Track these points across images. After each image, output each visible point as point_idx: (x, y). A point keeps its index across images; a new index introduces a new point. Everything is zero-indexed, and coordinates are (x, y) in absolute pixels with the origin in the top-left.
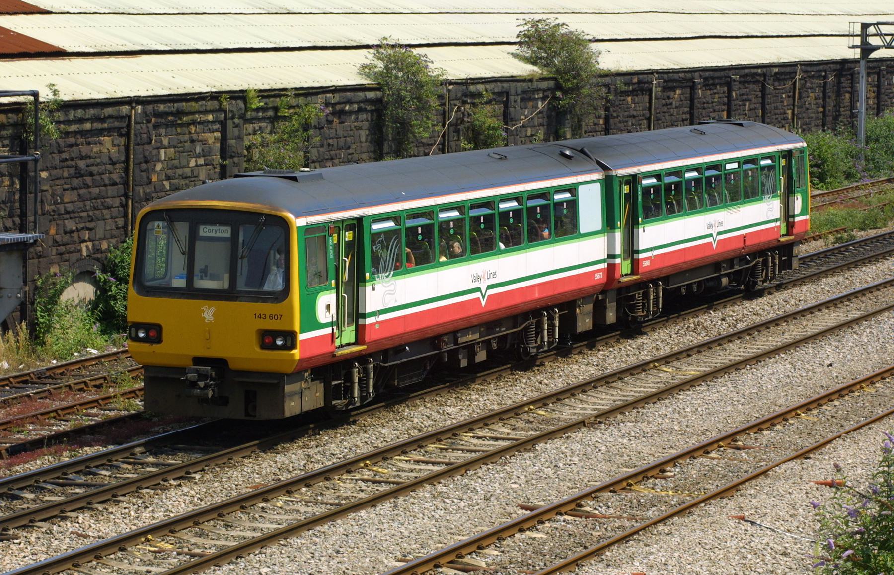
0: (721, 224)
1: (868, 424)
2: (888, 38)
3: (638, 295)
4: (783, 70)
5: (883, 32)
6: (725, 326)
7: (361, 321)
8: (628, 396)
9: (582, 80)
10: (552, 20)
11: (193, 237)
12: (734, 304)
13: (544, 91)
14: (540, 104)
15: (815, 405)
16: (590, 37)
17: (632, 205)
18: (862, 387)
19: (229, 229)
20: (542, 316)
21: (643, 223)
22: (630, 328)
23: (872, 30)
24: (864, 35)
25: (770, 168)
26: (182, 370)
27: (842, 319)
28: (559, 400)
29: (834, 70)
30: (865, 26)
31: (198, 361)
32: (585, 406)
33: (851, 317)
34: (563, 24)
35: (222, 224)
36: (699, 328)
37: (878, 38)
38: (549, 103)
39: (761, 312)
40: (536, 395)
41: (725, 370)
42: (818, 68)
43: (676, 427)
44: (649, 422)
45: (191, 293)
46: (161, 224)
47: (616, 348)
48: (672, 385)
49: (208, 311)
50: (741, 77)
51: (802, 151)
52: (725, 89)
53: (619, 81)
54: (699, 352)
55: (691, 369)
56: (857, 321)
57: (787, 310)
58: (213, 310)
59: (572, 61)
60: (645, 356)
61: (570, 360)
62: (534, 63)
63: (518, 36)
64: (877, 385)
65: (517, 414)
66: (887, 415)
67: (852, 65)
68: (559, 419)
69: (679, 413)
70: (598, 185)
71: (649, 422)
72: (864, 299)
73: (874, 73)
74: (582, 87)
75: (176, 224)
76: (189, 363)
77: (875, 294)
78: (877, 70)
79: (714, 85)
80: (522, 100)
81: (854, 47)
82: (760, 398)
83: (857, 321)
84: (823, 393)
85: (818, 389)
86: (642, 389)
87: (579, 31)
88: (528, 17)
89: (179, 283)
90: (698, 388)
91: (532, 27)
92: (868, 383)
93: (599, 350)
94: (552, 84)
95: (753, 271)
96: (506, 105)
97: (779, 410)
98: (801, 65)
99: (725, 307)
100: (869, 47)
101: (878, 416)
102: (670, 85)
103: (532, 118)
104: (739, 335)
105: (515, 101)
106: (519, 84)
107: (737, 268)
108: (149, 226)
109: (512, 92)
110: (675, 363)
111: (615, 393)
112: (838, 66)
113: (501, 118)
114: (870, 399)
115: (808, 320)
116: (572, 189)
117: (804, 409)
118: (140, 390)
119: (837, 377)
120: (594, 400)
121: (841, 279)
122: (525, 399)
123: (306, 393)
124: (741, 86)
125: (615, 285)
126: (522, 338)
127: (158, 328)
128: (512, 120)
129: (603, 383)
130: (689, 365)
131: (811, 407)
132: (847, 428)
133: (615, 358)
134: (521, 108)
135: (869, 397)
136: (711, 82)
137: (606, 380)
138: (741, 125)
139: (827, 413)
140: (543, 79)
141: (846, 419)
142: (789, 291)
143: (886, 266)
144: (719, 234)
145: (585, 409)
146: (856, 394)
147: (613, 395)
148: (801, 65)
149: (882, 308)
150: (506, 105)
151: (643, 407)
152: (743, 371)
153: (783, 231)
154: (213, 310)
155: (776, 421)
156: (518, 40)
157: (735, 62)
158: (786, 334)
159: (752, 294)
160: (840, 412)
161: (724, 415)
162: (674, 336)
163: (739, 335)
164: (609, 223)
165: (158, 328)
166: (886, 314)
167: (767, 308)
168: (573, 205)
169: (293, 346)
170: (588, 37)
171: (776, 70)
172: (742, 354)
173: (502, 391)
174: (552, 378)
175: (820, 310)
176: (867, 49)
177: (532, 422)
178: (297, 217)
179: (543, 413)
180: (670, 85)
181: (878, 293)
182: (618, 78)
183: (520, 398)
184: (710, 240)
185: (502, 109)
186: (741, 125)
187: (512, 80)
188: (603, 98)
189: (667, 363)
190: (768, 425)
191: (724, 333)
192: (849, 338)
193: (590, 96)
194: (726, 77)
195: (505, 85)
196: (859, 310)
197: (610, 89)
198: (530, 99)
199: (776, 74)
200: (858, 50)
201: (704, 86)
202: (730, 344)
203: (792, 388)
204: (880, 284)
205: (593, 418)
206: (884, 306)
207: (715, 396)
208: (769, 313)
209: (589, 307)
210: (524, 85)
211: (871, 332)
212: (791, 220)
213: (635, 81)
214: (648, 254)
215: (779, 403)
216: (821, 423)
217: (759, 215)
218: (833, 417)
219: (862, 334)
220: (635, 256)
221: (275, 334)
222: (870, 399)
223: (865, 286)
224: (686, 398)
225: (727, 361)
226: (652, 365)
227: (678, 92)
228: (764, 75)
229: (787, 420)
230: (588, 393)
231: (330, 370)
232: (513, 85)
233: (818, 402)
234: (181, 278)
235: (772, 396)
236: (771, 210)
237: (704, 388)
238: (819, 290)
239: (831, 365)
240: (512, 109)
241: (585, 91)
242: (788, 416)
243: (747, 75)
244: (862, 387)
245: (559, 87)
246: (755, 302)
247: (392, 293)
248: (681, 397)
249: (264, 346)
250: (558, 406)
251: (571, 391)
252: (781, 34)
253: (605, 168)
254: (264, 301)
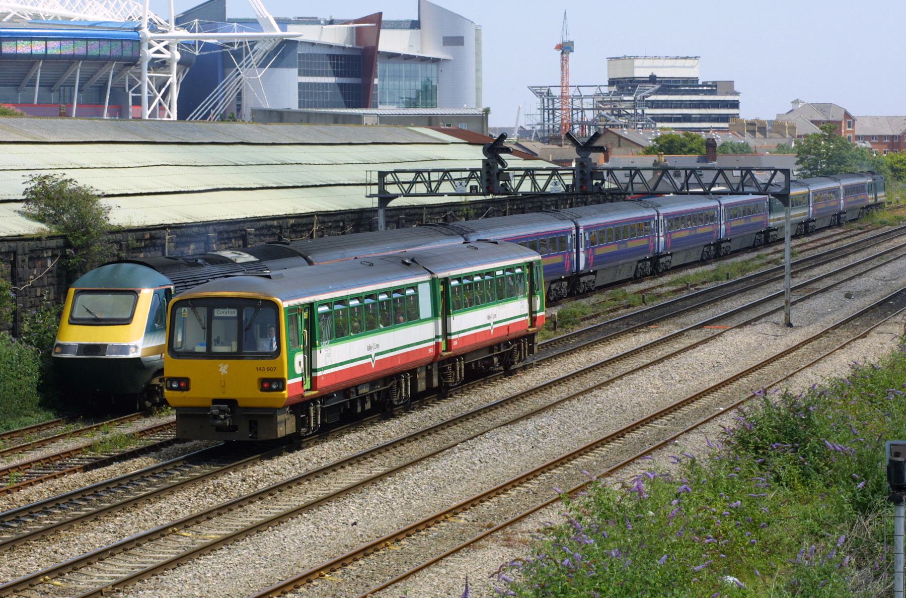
0: (378, 345)
1: (394, 583)
2: (406, 186)
3: (449, 366)
4: (299, 221)
5: (401, 180)
6: (246, 486)
7: (314, 374)
8: (146, 563)
9: (92, 237)
10: (59, 175)
11: (210, 317)
12: (254, 464)
13: (53, 249)
14: (49, 262)
15: (339, 565)
16: (99, 193)
17: (448, 300)
18: (387, 545)
19: (236, 311)
20: (401, 377)
21: (454, 313)
22: (442, 393)
23: (389, 178)
24: (382, 183)
25: (521, 274)
26: (208, 409)
27: (366, 475)
28: (75, 569)
29: (352, 220)
30: (382, 175)
31: (216, 401)
32: (103, 574)
33: (374, 473)
34: (71, 180)
35: (230, 307)
36: (219, 490)
37: (396, 186)
38: (59, 262)
39: (282, 471)
40: (51, 566)
41: (247, 532)
42: (335, 218)
43: (197, 593)
44: (169, 589)
45: (210, 355)
46: (186, 309)
47: (133, 513)
48: (192, 550)
49: (223, 367)
50: (256, 229)
51: (538, 262)
52: (241, 243)
53: (130, 237)
54: (220, 514)
55: (211, 532)
56: (381, 477)
57: (309, 468)
58: (226, 366)
59: (82, 217)
60: (163, 521)
61: (86, 527)
62: (42, 221)
63: (24, 194)
64: (403, 542)
65: (32, 586)
66: (413, 573)
67: (371, 215)
68: (75, 590)
69: (200, 578)
70: (428, 284)
71: (169, 589)
72: (387, 454)
73: (393, 222)
74: (92, 245)
75: (197, 308)
76: (209, 403)
77: (399, 449)
78: (396, 218)
79: (230, 239)
80: (31, 259)
81: (371, 196)
82: (283, 561)
83: (381, 477)
84: (347, 552)
85: (342, 549)
86: (161, 555)
87: (88, 187)
88: (34, 174)
89: (201, 349)
90: (219, 552)
91: (39, 184)
92: (393, 540)
93: (116, 516)
94: (61, 242)
95: (511, 354)
96: (14, 264)
97: (303, 572)
98: (318, 215)
99: (245, 467)
100: (387, 195)
101: (404, 574)
102: (183, 239)
103: (41, 278)
104: (259, 496)
105: (23, 261)
106: (26, 243)
107: (503, 350)
108: (178, 311)
109: (20, 251)
110: (195, 527)
111: (133, 560)
112: (356, 216)
113: (9, 278)
114: (396, 557)
115: (330, 478)
116: (414, 287)
117: (328, 570)
118: (173, 423)
119: (361, 535)
120: (111, 568)
121: (364, 434)
122: (40, 569)
123: (288, 422)
124: (257, 239)
125: (439, 358)
126: (388, 393)
127: (187, 380)
128: (20, 280)
129: (121, 550)
130: (209, 528)
131: (335, 567)
132: (373, 588)
133: (132, 523)
134: (30, 268)
135: (394, 555)
136: (226, 236)
137: (125, 547)
138: (269, 277)
139: (352, 573)
140: (51, 237)
141: (372, 578)
142: (311, 449)
143: (410, 420)
144: (377, 354)
145: (103, 578)
146: (382, 552)
147: (131, 563)
148: (318, 215)
149: (406, 463)
150: (14, 264)
151: (163, 574)
152: (264, 533)
153: (307, 386)
154: (226, 366)
155: (299, 584)
156: (24, 197)
157: (250, 215)
158: (309, 493)
159: (509, 373)
160: (366, 572)
161: (246, 579)
162: (193, 499)
163: (259, 496)
164: (435, 315)
165: (187, 380)
166: (411, 469)
167: (288, 467)
168: (416, 296)
169: (283, 389)
170: (97, 193)
171: (292, 221)
172: (263, 515)
173: (16, 562)
174: (68, 546)
175: (343, 467)
176: (385, 198)
177: (47, 593)
178: (283, 301)
179: (59, 583)
180: (183, 239)
181: (402, 448)
182: (130, 234)
183: (35, 570)
184: (489, 328)
185: (10, 269)
186: (269, 277)
187: (20, 238)
188: (114, 255)
189: (186, 527)
190: (291, 587)
191: (245, 494)
192: (373, 495)
193: (100, 253)
194: (241, 230)
195: (12, 244)
196: (383, 466)
197: (121, 245)
198: (39, 258)
199: (293, 225)
200: (376, 199)
201: (219, 240)
202: (252, 505)
203: (315, 549)
204: (404, 439)
205: (110, 587)
206: (409, 461)
207: (236, 560)
208: (290, 472)
209: (424, 374)
210: (32, 243)
211: (395, 488)
212: (534, 315)
213: (147, 236)
214: (326, 372)
215: (302, 565)
216: (346, 584)
217: (512, 311)
218: (358, 577)
219: (386, 490)
220: (449, 338)
221: (270, 381)
222: (396, 557)
223: (389, 440)
224: (207, 563)
225: (248, 524)
226: (170, 530)
227: (192, 247)
228: (280, 227)
229: (311, 582)
230: (106, 561)
231: (299, 407)
232: (20, 244)
233: (342, 562)
234: (202, 345)
235: (294, 557)
236: (329, 355)
237: (225, 551)
238: (342, 446)
239: (355, 524)
240: (20, 269)
241: (96, 248)
242: (312, 578)
243: (262, 228)
244: (387, 545)
245: (68, 245)
246: (276, 461)
247: (329, 355)
248: (201, 562)
249: (263, 389)
250: (75, 576)
251: (87, 560)
252: (296, 184)
253: (431, 273)
254: (263, 358)
